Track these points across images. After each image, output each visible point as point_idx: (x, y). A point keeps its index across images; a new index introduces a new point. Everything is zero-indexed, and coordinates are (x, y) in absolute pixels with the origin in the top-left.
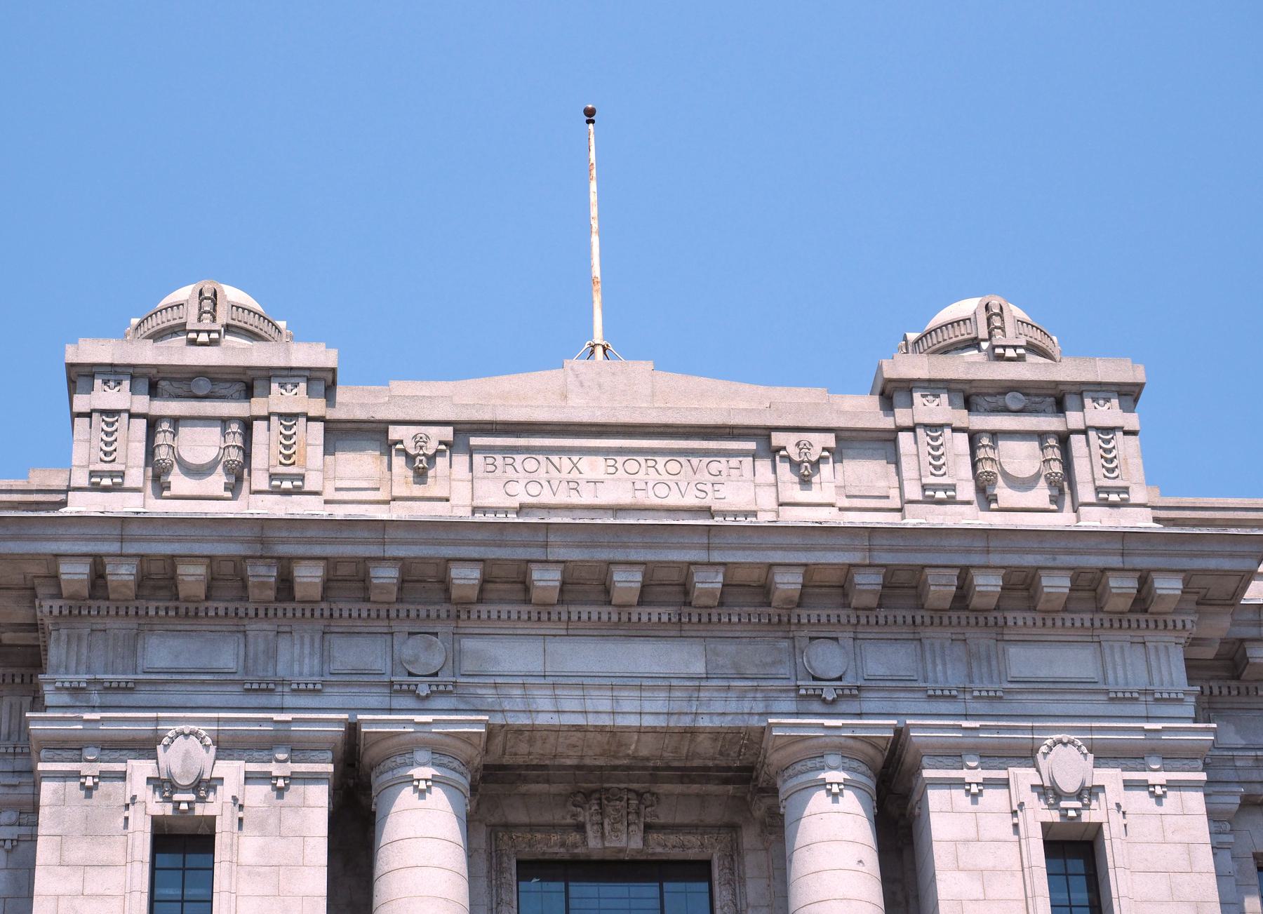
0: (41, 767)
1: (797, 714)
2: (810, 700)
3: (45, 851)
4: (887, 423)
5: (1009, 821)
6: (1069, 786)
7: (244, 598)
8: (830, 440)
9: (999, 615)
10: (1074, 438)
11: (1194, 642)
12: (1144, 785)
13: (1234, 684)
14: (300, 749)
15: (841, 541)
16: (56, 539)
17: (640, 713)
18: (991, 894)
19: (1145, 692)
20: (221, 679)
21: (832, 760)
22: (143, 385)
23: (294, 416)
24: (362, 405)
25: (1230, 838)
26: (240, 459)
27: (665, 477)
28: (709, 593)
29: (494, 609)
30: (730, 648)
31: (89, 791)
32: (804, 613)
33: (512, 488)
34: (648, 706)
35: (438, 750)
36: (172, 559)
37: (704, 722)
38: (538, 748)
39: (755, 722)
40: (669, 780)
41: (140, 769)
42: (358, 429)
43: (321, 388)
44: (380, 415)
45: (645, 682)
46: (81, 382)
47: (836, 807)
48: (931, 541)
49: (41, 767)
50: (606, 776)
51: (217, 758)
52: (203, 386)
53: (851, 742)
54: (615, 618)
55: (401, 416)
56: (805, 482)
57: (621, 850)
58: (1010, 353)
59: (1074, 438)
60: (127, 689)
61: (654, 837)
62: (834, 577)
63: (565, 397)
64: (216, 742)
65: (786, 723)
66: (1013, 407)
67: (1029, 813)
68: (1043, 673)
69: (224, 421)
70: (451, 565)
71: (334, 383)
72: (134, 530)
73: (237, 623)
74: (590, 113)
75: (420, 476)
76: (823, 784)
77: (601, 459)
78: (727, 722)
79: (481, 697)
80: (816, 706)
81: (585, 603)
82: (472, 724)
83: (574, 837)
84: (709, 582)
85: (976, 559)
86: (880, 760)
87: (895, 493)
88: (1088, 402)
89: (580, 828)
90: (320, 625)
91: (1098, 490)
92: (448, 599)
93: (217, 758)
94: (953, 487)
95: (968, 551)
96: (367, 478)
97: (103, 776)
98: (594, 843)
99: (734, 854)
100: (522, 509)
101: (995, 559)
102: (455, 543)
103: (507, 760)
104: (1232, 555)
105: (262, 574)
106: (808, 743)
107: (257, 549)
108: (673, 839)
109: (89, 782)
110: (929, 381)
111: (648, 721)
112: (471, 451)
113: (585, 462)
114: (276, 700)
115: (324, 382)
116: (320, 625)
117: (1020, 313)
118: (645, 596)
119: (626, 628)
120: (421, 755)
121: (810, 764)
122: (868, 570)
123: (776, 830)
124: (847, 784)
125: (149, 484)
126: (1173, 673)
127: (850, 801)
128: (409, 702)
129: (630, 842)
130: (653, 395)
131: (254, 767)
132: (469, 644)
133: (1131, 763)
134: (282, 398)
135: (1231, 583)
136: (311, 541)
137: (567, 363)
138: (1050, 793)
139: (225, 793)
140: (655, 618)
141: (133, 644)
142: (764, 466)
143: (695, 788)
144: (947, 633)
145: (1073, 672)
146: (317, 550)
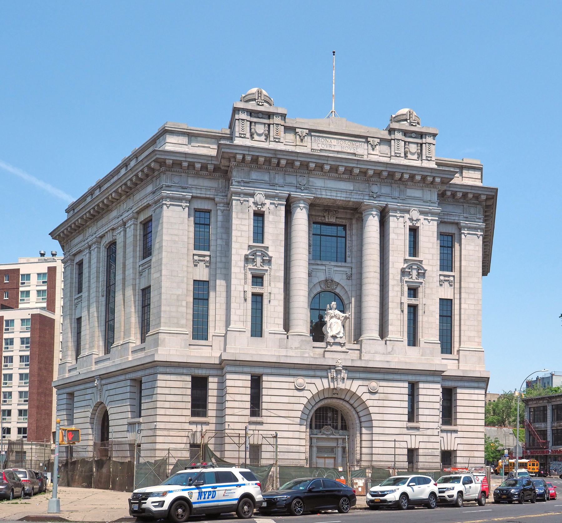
2: (372, 197)
3: (234, 215)
4: (389, 138)
5: (403, 224)
6: (415, 219)
7: (270, 165)
8: (378, 140)
12: (427, 219)
14: (280, 198)
15: (382, 165)
16: (237, 150)
17: (341, 197)
23: (278, 124)
30: (357, 185)
35: (304, 200)
37: (352, 200)
38: (321, 201)
39: (361, 201)
41: (251, 200)
44: (295, 126)
46: (237, 112)
48: (397, 167)
52: (260, 115)
56: (373, 149)
58: (414, 124)
60: (248, 183)
61: (337, 220)
62: (378, 172)
63: (329, 125)
65: (367, 201)
68: (413, 195)
69: (265, 124)
72: (251, 149)
73: (268, 171)
74: (334, 52)
75: (302, 140)
80: (372, 198)
82: (311, 196)
83: (323, 218)
85: (405, 171)
87: (389, 153)
89: (324, 217)
90: (283, 172)
91: (426, 157)
92: (308, 169)
94: (245, 134)
98: (327, 220)
99: (351, 224)
100: (321, 150)
101: (408, 172)
102: (311, 158)
105: (275, 161)
108: (340, 220)
111: (342, 199)
112: (311, 136)
113: (333, 141)
114: (275, 188)
115: (283, 116)
116: (283, 172)
117: (415, 114)
119: (340, 179)
123: (361, 221)
124: (376, 214)
126: (435, 198)
128: (299, 190)
129: (333, 220)
131: (272, 201)
132: (311, 179)
134: (277, 120)
136: (284, 155)
138: (411, 220)
141: (249, 173)
142: (366, 145)
145: (418, 196)
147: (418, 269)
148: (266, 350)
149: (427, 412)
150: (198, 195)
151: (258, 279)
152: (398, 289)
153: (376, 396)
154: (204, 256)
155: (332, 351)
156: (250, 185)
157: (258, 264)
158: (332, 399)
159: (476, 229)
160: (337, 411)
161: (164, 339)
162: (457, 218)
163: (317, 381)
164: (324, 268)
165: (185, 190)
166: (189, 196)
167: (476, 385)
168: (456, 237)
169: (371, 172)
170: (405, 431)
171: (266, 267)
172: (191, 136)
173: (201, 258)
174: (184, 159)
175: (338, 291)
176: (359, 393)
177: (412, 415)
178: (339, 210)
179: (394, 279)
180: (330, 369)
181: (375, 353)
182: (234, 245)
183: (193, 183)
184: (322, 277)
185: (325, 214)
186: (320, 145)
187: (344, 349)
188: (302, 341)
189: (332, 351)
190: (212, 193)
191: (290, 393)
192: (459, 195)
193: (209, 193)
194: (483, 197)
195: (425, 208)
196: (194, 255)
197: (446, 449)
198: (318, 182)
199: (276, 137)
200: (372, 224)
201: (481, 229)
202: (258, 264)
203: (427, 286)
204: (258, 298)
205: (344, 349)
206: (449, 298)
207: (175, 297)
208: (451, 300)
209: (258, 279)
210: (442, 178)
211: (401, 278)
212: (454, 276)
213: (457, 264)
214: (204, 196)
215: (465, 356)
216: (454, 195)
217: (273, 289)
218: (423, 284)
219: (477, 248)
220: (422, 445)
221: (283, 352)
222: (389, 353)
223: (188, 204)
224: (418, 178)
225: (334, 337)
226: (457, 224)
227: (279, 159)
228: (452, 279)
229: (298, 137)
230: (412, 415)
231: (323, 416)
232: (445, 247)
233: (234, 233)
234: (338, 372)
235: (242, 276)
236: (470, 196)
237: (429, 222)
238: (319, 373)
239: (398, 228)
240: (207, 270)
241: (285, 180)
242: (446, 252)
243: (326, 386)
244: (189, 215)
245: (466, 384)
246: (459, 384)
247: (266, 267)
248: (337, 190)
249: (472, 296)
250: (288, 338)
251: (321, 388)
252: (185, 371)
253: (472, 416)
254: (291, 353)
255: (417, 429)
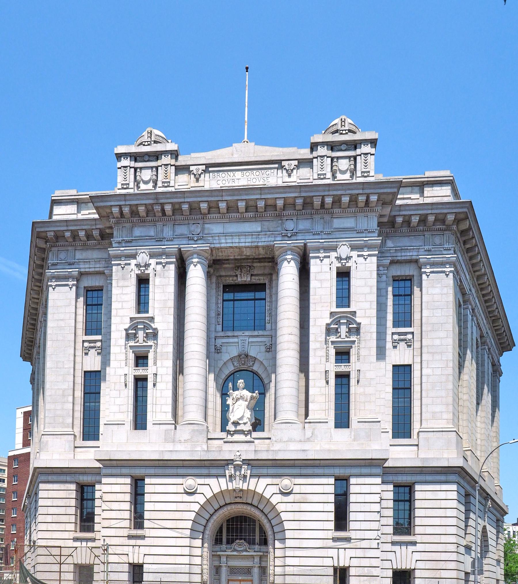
0: (113, 262)
1: (282, 241)
3: (114, 283)
4: (311, 156)
6: (344, 257)
9: (332, 210)
10: (358, 157)
11: (381, 216)
12: (362, 256)
13: (393, 229)
14: (168, 256)
17: (245, 242)
18: (323, 286)
19: (365, 230)
20: (151, 238)
21: (289, 252)
22: (133, 158)
24: (184, 161)
25: (386, 272)
26: (156, 178)
27: (256, 176)
28: (261, 207)
29: (212, 215)
30: (266, 223)
31: (123, 268)
32: (285, 212)
33: (219, 182)
34: (247, 240)
35: (199, 254)
36: (137, 205)
37: (260, 244)
39: (272, 243)
40: (256, 262)
41: (133, 262)
42: (183, 168)
43: (174, 156)
45: (247, 234)
47: (289, 265)
49: (113, 262)
50: (242, 263)
51: (150, 258)
53: (293, 248)
54: (240, 217)
55: (193, 163)
56: (289, 176)
57: (246, 281)
59: (358, 157)
61: (253, 277)
64: (150, 255)
65: (279, 243)
66: (343, 149)
67: (333, 264)
69: (152, 168)
70: (201, 203)
71: (178, 155)
73: (154, 223)
74: (247, 68)
76: (286, 259)
77: (240, 172)
78: (265, 244)
79: (209, 240)
80: (286, 238)
81: (233, 213)
82: (206, 247)
83: (235, 278)
84: (261, 204)
86: (301, 253)
88: (362, 145)
89: (237, 276)
90: (173, 223)
92: (201, 214)
93: (150, 258)
95: (324, 191)
96: (186, 182)
97: (126, 264)
100: (221, 187)
101: (331, 193)
102: (200, 197)
103: (218, 258)
104: (391, 188)
106: (283, 248)
107: (155, 201)
108: (257, 278)
109: (123, 266)
110: (322, 142)
111: (247, 244)
114: (163, 243)
115: (175, 154)
116: (173, 223)
117: (350, 121)
118: (247, 210)
119: (243, 220)
120: (195, 256)
121: (284, 254)
122: (300, 198)
125: (136, 187)
126: (373, 224)
127: (292, 263)
128: (193, 242)
130: (254, 153)
131: (158, 260)
132: (206, 226)
133: (360, 250)
134: (166, 160)
135: (390, 197)
136: (168, 198)
137: (234, 145)
139: (152, 267)
140: (249, 216)
143: (262, 264)
144: (319, 216)
146: (169, 201)
147: (349, 323)
148: (148, 445)
149: (361, 516)
150: (87, 270)
151: (141, 359)
152: (323, 353)
153: (291, 498)
154: (95, 341)
155: (231, 442)
156: (133, 244)
157: (141, 341)
158: (236, 505)
159: (443, 264)
160: (254, 521)
161: (47, 442)
162: (415, 254)
163: (213, 481)
164: (236, 340)
165: (72, 266)
166: (75, 272)
167: (443, 478)
168: (416, 279)
169: (280, 203)
170: (331, 543)
171: (150, 343)
172: (78, 202)
173: (92, 345)
174: (65, 228)
175: (255, 368)
176: (267, 495)
177: (341, 519)
178: (255, 265)
179: (316, 341)
180: (228, 465)
181: (285, 440)
182: (114, 320)
183: (81, 257)
184: (234, 352)
185: (238, 273)
186: (219, 182)
187: (248, 438)
188: (193, 431)
189: (231, 442)
190: (101, 266)
191: (178, 498)
192: (415, 220)
193: (98, 266)
194: (451, 218)
195: (359, 241)
196: (83, 341)
197: (399, 567)
198: (216, 229)
199: (165, 180)
200: (288, 272)
201: (452, 264)
202: (141, 341)
203: (362, 345)
204: (140, 382)
205: (248, 438)
206: (406, 363)
207: (61, 392)
208: (410, 365)
209: (141, 359)
210: (379, 194)
211: (326, 338)
212: (413, 333)
213: (416, 316)
214: (93, 270)
215: (427, 439)
216: (407, 222)
217: (160, 367)
218: (356, 343)
219: (445, 290)
220: (355, 562)
221: (170, 447)
222: (308, 440)
223: (75, 282)
224: (345, 200)
225: (236, 424)
226: (416, 261)
227: (162, 205)
228: (410, 336)
229: (192, 176)
230: (341, 519)
231: (237, 528)
232: (401, 295)
233: (114, 306)
234: (238, 468)
235: (123, 357)
236: (431, 218)
237: (366, 259)
238: (213, 471)
239: (323, 273)
240: (99, 358)
241: (174, 231)
242: (402, 302)
243: (224, 487)
244: (77, 297)
245: (429, 478)
246: (418, 478)
247: (150, 343)
248: (240, 234)
249: (437, 357)
250: (176, 429)
251: (216, 490)
252: (68, 478)
253: (437, 521)
254: (179, 447)
255: (348, 540)
